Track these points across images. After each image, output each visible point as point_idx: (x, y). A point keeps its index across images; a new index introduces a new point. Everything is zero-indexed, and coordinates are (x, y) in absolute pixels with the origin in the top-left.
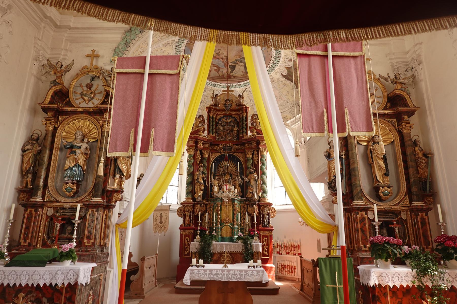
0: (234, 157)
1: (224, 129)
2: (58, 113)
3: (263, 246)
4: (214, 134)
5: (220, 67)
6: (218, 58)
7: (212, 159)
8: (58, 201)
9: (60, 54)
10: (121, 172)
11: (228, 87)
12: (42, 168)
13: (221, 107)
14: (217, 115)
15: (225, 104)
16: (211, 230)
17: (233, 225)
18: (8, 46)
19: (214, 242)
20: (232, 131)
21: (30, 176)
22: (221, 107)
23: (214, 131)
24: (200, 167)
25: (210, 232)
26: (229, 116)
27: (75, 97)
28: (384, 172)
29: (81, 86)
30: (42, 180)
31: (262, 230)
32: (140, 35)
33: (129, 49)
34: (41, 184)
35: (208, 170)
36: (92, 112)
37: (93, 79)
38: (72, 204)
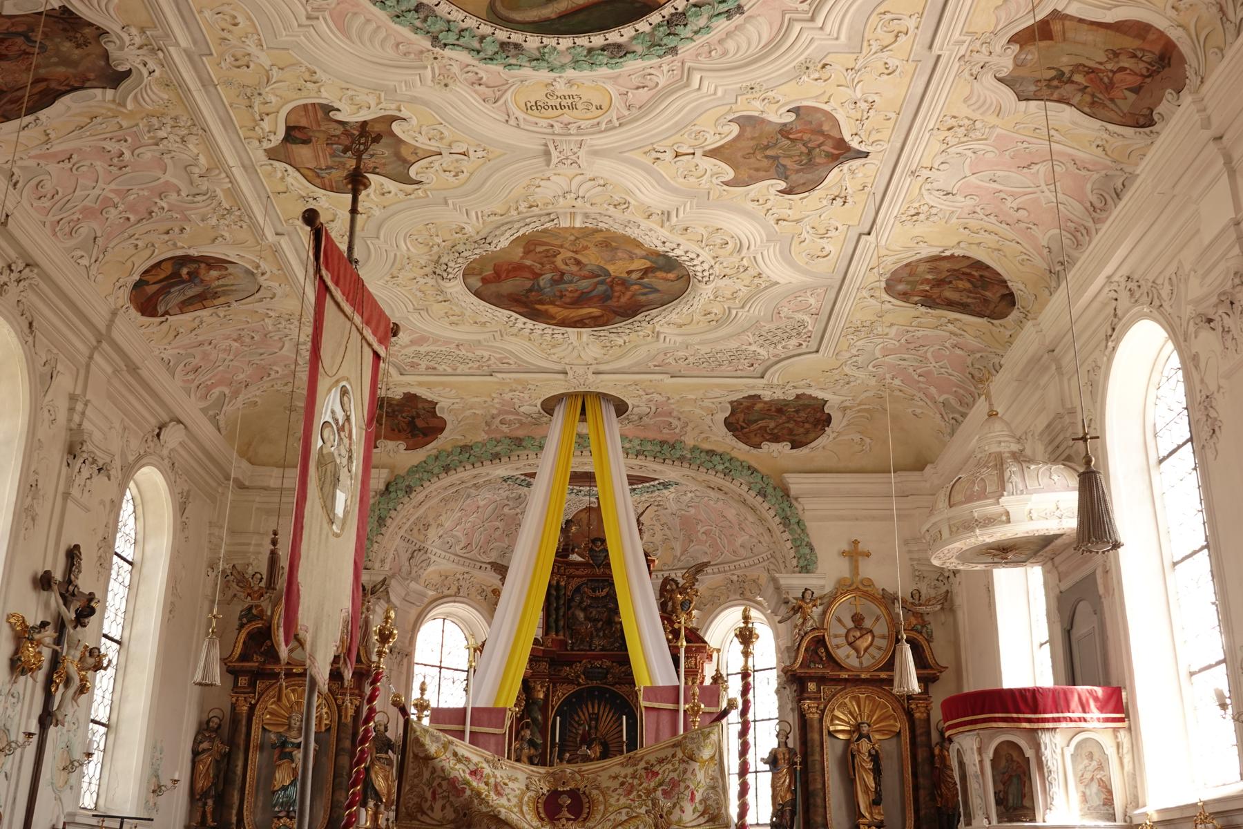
1: (587, 618)
2: (255, 676)
4: (561, 633)
7: (556, 702)
9: (249, 544)
18: (72, 451)
21: (210, 802)
23: (562, 623)
24: (522, 728)
28: (872, 797)
30: (234, 812)
32: (406, 500)
34: (234, 819)
35: (543, 733)
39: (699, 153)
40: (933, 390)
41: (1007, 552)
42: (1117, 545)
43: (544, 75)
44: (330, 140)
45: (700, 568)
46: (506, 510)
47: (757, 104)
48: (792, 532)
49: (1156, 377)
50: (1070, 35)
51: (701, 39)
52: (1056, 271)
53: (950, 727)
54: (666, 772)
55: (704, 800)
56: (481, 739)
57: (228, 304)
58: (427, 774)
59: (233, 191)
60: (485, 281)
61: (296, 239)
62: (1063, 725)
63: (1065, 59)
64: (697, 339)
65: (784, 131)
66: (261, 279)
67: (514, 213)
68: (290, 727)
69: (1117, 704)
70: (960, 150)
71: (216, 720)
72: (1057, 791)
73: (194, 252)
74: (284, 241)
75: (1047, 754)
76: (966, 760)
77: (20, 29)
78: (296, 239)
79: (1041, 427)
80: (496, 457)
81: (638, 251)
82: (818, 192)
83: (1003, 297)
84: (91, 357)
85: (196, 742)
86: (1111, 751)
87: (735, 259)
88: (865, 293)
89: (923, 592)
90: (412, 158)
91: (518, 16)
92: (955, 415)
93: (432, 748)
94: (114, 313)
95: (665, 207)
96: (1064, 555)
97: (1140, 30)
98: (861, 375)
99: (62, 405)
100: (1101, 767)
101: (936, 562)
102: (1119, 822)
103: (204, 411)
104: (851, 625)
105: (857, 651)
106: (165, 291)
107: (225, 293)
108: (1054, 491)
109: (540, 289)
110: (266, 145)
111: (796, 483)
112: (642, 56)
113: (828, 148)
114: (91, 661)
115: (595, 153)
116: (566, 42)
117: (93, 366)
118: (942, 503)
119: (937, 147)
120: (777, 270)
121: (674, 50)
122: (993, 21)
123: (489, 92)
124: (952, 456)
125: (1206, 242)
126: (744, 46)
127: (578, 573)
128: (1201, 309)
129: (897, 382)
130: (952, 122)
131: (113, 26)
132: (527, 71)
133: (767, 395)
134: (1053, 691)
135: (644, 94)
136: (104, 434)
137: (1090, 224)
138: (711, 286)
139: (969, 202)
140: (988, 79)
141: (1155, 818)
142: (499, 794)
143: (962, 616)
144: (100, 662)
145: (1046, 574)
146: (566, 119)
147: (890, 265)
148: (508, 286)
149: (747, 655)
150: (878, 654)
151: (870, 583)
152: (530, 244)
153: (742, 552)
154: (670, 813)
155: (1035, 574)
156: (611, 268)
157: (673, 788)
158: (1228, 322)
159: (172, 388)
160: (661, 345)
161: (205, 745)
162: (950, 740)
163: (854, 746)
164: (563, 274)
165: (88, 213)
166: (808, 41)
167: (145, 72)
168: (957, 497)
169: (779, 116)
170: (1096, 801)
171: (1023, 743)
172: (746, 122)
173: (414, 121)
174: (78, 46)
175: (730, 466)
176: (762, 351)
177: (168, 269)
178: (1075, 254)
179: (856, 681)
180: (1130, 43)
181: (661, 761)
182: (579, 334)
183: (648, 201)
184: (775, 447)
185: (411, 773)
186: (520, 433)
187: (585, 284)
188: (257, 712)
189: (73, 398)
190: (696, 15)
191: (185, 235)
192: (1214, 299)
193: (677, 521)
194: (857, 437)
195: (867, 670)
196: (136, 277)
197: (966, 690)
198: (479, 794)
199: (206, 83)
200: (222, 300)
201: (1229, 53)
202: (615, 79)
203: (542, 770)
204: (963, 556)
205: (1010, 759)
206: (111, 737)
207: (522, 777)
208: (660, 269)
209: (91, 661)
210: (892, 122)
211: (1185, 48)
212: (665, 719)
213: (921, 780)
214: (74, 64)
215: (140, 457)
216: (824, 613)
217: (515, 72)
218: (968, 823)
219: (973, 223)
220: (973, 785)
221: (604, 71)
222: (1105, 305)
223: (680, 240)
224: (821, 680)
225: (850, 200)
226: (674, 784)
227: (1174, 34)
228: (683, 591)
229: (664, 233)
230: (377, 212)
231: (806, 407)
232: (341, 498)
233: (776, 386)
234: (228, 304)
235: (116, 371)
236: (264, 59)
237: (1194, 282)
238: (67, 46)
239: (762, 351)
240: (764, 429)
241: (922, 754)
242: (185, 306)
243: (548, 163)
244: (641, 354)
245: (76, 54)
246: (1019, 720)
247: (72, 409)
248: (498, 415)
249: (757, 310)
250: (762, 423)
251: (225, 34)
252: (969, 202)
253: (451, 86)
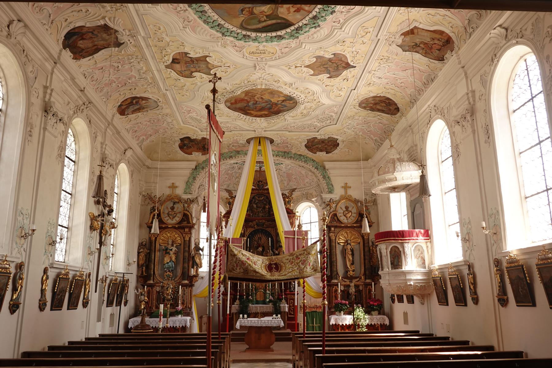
0: (266, 231)
1: (257, 207)
3: (290, 307)
10: (197, 265)
16: (248, 295)
17: (265, 291)
19: (250, 305)
20: (264, 208)
21: (144, 268)
25: (247, 297)
29: (167, 208)
31: (288, 294)
37: (174, 203)
39: (303, 66)
40: (372, 136)
41: (394, 189)
42: (430, 196)
43: (256, 44)
44: (186, 63)
45: (294, 190)
46: (229, 172)
47: (322, 53)
48: (326, 180)
49: (442, 136)
50: (419, 33)
51: (306, 34)
52: (413, 102)
53: (377, 242)
54: (302, 258)
55: (313, 265)
57: (147, 111)
58: (235, 260)
59: (153, 78)
60: (232, 104)
61: (172, 91)
62: (411, 241)
63: (418, 40)
64: (298, 121)
65: (330, 60)
66: (159, 104)
67: (243, 84)
68: (168, 244)
69: (427, 235)
70: (384, 65)
72: (409, 260)
73: (138, 96)
74: (168, 93)
75: (406, 249)
76: (382, 251)
77: (91, 31)
78: (172, 91)
79: (406, 149)
80: (231, 157)
81: (281, 95)
82: (340, 77)
83: (396, 108)
84: (106, 130)
85: (139, 249)
86: (425, 248)
87: (312, 97)
88: (352, 107)
89: (367, 199)
90: (212, 68)
91: (249, 27)
92: (379, 144)
93: (236, 252)
94: (113, 116)
95: (291, 82)
96: (413, 189)
97: (441, 33)
98: (349, 131)
99: (99, 146)
100: (422, 253)
101: (373, 192)
102: (427, 269)
103: (138, 144)
104: (344, 209)
105: (347, 217)
106: (128, 107)
107: (146, 108)
108: (410, 171)
109: (249, 106)
110: (165, 64)
111: (328, 165)
112: (288, 39)
113: (343, 65)
114: (111, 226)
115: (270, 66)
116: (264, 35)
117: (107, 133)
118: (376, 174)
119: (377, 64)
120: (325, 101)
121: (298, 37)
122: (396, 28)
123: (238, 49)
124: (378, 156)
125: (459, 98)
126: (319, 36)
128: (456, 119)
129: (361, 133)
130: (382, 58)
131: (120, 29)
132: (251, 43)
133: (319, 137)
134: (409, 231)
135: (287, 49)
136: (112, 156)
137: (423, 88)
138: (304, 105)
139: (386, 81)
140: (394, 46)
141: (437, 268)
142: (255, 265)
143: (380, 207)
144: (114, 226)
145: (407, 195)
146: (262, 56)
147: (361, 99)
148: (239, 105)
149: (309, 218)
150: (353, 219)
151: (351, 196)
152: (247, 93)
153: (307, 185)
154: (303, 269)
155: (403, 195)
156: (272, 100)
157: (304, 262)
158: (464, 123)
159: (128, 137)
160: (286, 123)
161: (142, 250)
162: (377, 245)
163: (346, 247)
164: (257, 102)
165: (106, 85)
166: (339, 35)
167: (129, 43)
168: (381, 172)
169: (328, 56)
170: (421, 263)
171: (399, 246)
172: (318, 57)
173: (214, 57)
174: (108, 35)
175: (306, 159)
176: (318, 124)
177: (129, 101)
178: (419, 97)
179: (346, 227)
180: (437, 36)
181: (300, 255)
182: (261, 120)
183: (286, 80)
184: (321, 153)
185: (230, 259)
186: (239, 149)
187: (264, 105)
188: (157, 240)
189: (102, 143)
190: (305, 27)
191: (136, 90)
192: (460, 116)
193: (286, 174)
194: (347, 150)
195: (349, 223)
196: (119, 104)
197: (380, 231)
198: (250, 265)
199: (148, 46)
200: (146, 110)
201: (468, 42)
202: (278, 45)
203: (266, 258)
204: (382, 190)
205: (395, 251)
206: (114, 249)
207: (261, 260)
208: (288, 100)
209: (111, 226)
210: (363, 58)
211: (454, 38)
212: (291, 240)
213: (366, 257)
214: (106, 40)
215: (120, 161)
216: (336, 206)
217: (248, 43)
218: (382, 270)
219: (387, 87)
220: (384, 259)
221: (276, 43)
222: (427, 113)
223: (295, 91)
224: (336, 227)
225: (349, 80)
226: (304, 261)
227: (451, 35)
228: (288, 197)
229: (290, 90)
230: (199, 84)
231: (331, 141)
232: (216, 184)
233: (321, 135)
234: (147, 111)
235: (113, 134)
236: (168, 39)
237: (454, 110)
238: (105, 35)
239: (318, 124)
240: (317, 148)
241: (366, 249)
242: (134, 112)
243: (255, 69)
244: (280, 125)
245: (107, 37)
246: (398, 240)
247: (102, 147)
248: (232, 143)
249: (318, 112)
250: (317, 146)
251: (156, 32)
252: (386, 81)
253: (227, 47)
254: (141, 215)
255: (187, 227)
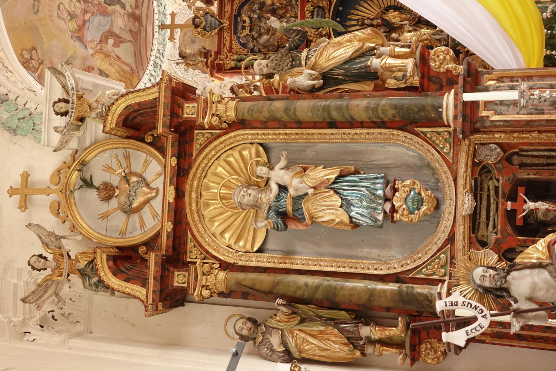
5: (107, 28)
6: (84, 22)
8: (451, 239)
11: (163, 27)
12: (343, 288)
13: (211, 44)
14: (230, 52)
15: (204, 29)
21: (365, 331)
22: (211, 44)
26: (236, 23)
27: (135, 229)
29: (104, 216)
33: (12, 97)
34: (392, 287)
36: (178, 158)
37: (87, 183)
38: (460, 189)
56: (453, 255)
68: (256, 206)
71: (239, 324)
127: (227, 44)
254: (127, 341)
255: (174, 112)
